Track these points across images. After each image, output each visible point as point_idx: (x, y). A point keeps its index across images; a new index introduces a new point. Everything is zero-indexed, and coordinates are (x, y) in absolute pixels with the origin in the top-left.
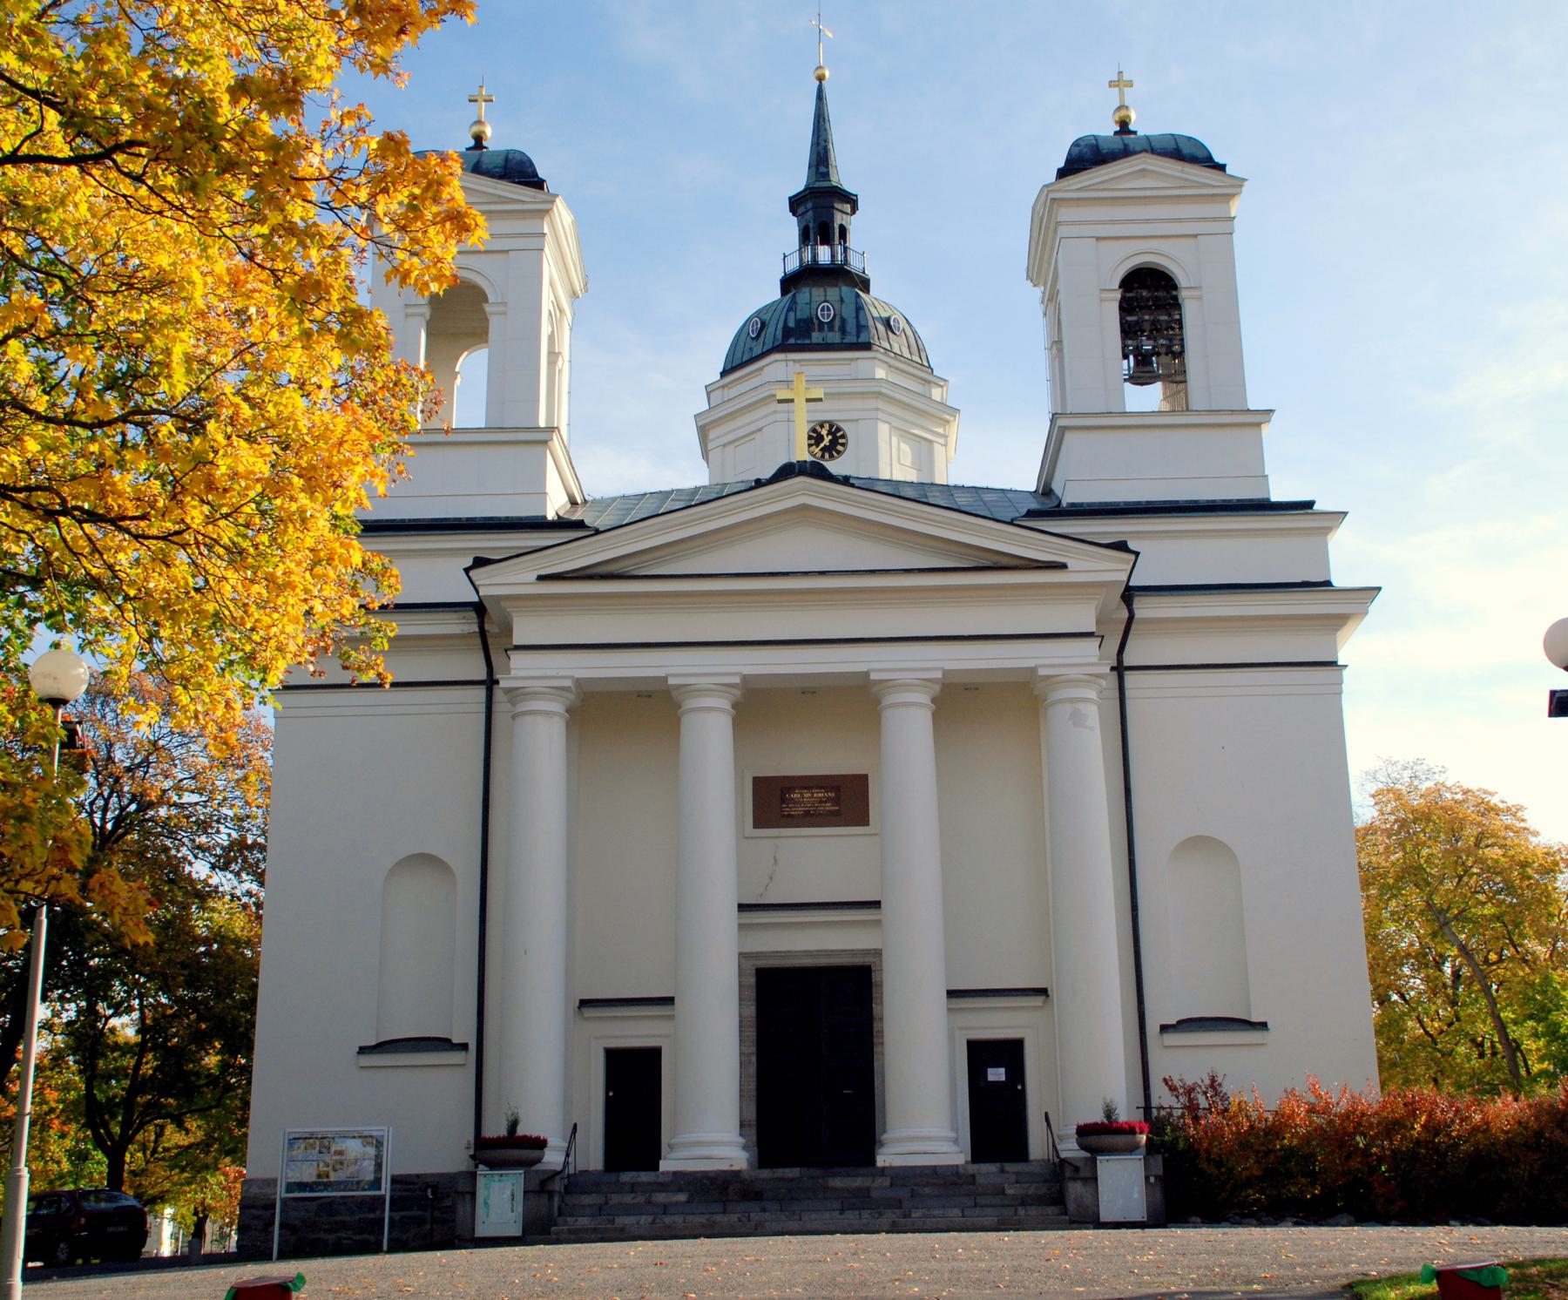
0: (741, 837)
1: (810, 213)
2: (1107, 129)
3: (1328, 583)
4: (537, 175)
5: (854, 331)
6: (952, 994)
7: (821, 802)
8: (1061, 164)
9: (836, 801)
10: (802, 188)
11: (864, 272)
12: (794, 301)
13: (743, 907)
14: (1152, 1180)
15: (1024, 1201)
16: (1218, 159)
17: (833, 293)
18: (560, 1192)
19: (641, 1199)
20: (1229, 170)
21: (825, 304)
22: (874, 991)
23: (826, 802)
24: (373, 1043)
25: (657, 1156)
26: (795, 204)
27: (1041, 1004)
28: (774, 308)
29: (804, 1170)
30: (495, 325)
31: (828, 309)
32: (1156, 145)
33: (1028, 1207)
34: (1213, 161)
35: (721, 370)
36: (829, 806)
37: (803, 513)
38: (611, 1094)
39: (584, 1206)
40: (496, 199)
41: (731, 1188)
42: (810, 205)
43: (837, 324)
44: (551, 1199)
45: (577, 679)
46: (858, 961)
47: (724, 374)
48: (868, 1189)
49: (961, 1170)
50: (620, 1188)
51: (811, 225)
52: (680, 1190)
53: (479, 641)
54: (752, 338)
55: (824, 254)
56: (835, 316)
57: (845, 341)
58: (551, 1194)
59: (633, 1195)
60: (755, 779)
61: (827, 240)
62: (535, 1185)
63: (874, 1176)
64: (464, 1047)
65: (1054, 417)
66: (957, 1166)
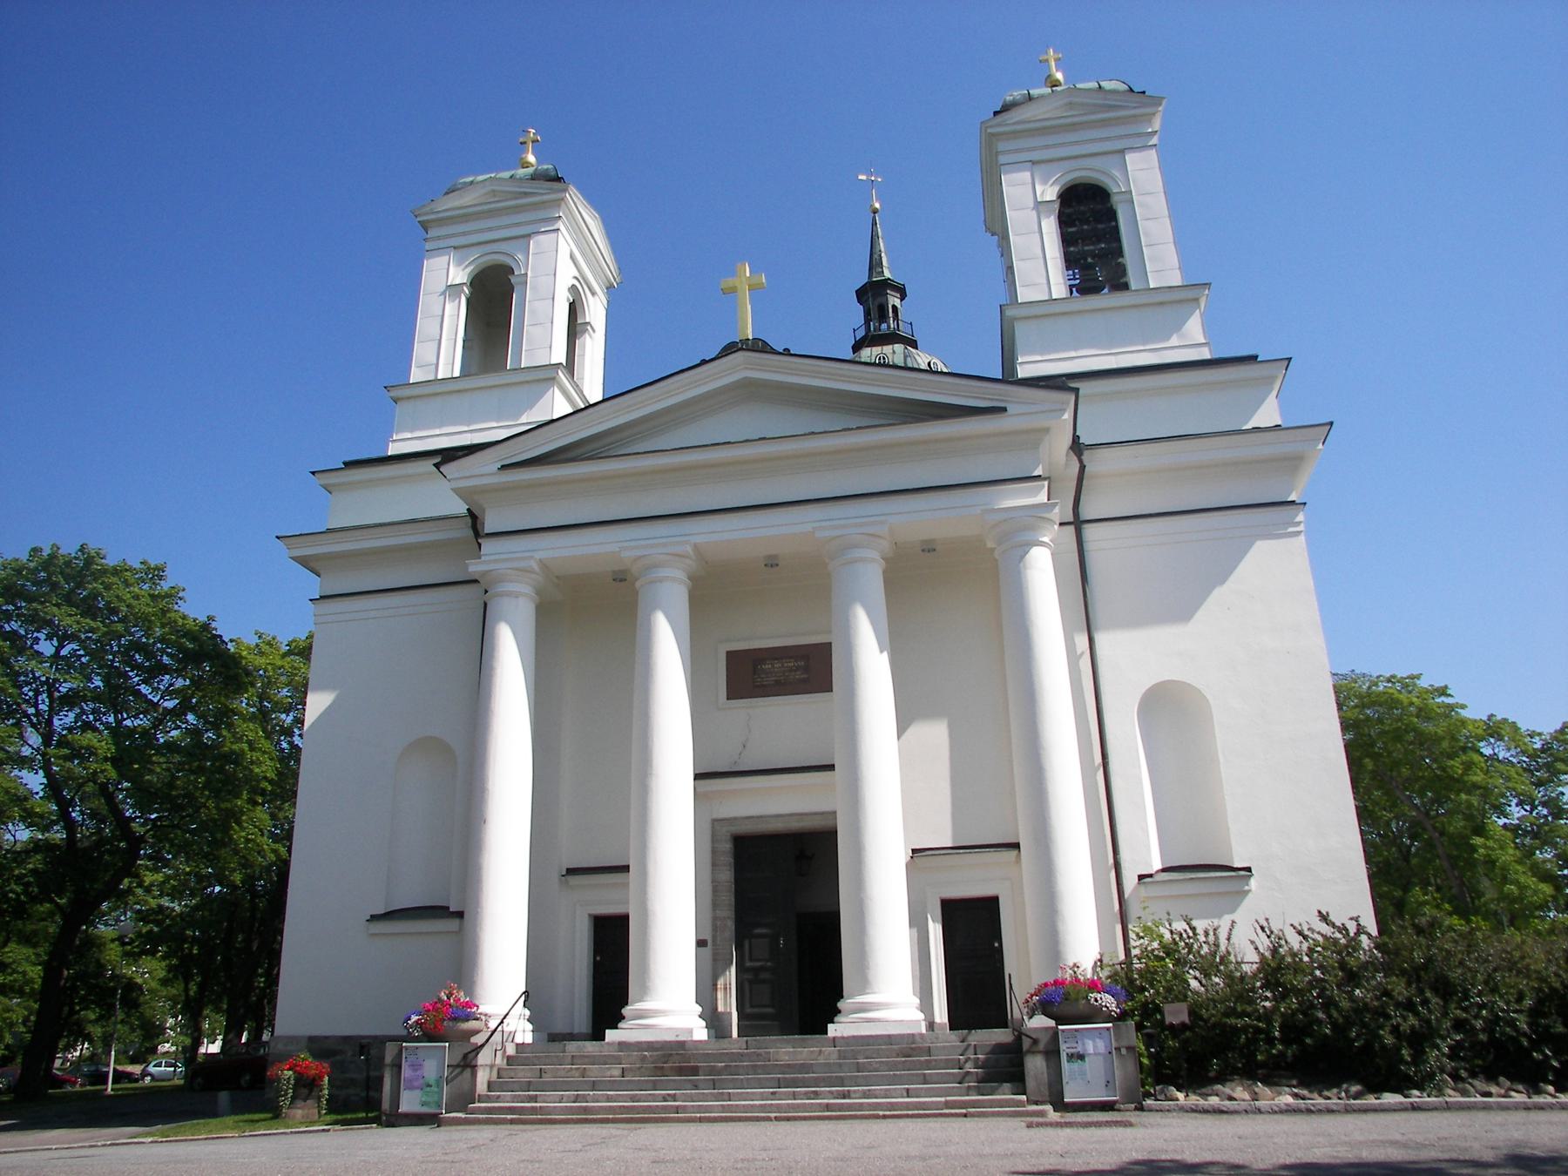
7: (791, 671)
14: (1124, 1051)
22: (733, 900)
23: (795, 671)
31: (884, 358)
36: (799, 675)
38: (598, 958)
60: (728, 652)
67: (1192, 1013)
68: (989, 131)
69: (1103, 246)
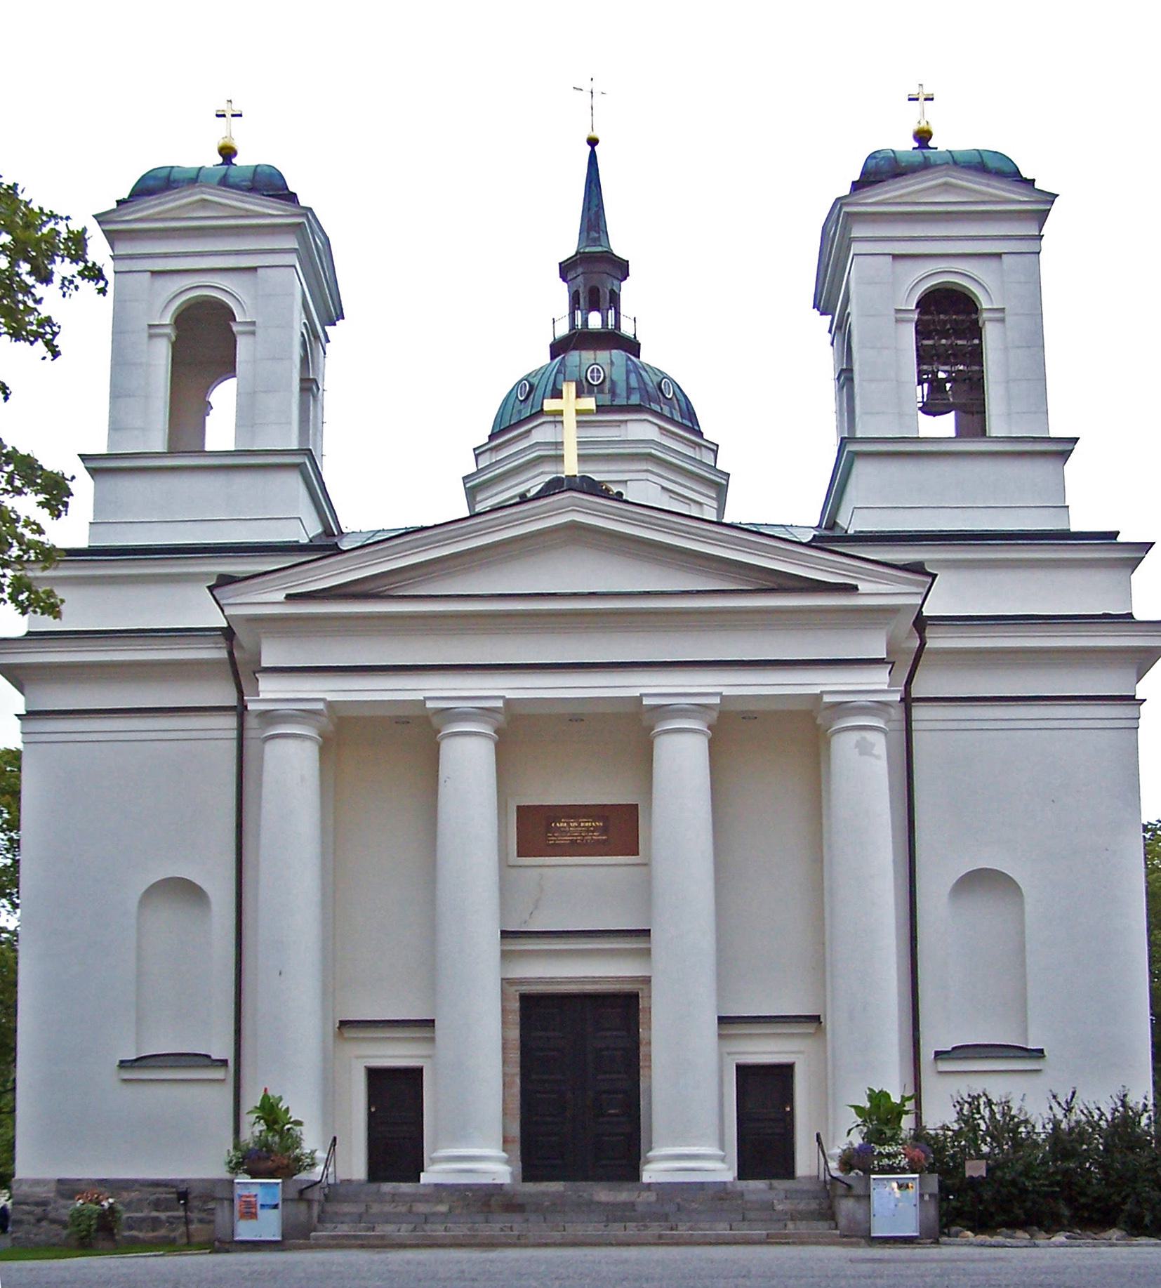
0: (504, 865)
1: (580, 279)
2: (905, 144)
3: (1130, 616)
4: (287, 189)
5: (624, 394)
6: (722, 1020)
7: (588, 831)
8: (857, 178)
9: (604, 830)
10: (573, 253)
11: (635, 337)
12: (562, 362)
13: (505, 934)
14: (927, 1197)
15: (795, 1216)
16: (1026, 173)
17: (603, 356)
18: (319, 1201)
19: (403, 1209)
20: (1037, 185)
21: (595, 366)
23: (593, 832)
24: (134, 1058)
25: (420, 1168)
26: (566, 270)
27: (812, 1031)
28: (543, 371)
29: (568, 1184)
30: (244, 349)
32: (960, 159)
33: (798, 1223)
34: (1021, 176)
35: (489, 433)
37: (576, 535)
39: (345, 1214)
40: (242, 213)
41: (493, 1199)
42: (580, 270)
43: (607, 385)
44: (310, 1207)
45: (330, 702)
46: (627, 987)
47: (492, 437)
48: (633, 1204)
49: (729, 1186)
50: (381, 1198)
51: (581, 291)
52: (441, 1202)
53: (228, 667)
54: (521, 401)
55: (595, 320)
56: (605, 377)
57: (615, 403)
58: (310, 1202)
59: (394, 1205)
60: (518, 807)
61: (594, 305)
62: (293, 1193)
63: (640, 1191)
64: (224, 1063)
65: (843, 442)
66: (725, 1183)
67: (989, 1170)
68: (845, 209)
69: (961, 368)
